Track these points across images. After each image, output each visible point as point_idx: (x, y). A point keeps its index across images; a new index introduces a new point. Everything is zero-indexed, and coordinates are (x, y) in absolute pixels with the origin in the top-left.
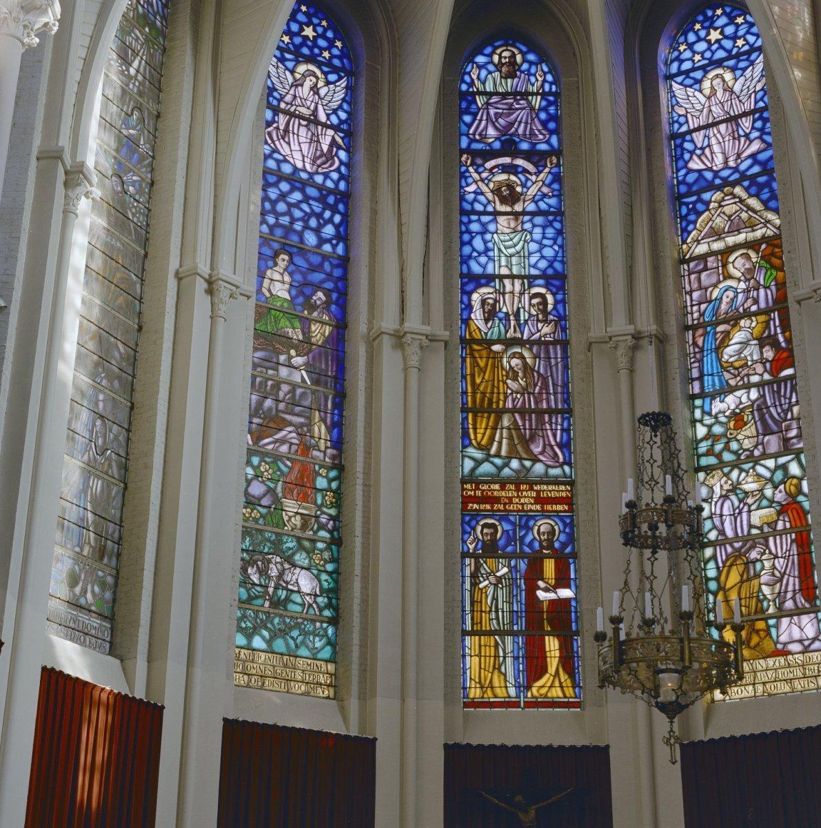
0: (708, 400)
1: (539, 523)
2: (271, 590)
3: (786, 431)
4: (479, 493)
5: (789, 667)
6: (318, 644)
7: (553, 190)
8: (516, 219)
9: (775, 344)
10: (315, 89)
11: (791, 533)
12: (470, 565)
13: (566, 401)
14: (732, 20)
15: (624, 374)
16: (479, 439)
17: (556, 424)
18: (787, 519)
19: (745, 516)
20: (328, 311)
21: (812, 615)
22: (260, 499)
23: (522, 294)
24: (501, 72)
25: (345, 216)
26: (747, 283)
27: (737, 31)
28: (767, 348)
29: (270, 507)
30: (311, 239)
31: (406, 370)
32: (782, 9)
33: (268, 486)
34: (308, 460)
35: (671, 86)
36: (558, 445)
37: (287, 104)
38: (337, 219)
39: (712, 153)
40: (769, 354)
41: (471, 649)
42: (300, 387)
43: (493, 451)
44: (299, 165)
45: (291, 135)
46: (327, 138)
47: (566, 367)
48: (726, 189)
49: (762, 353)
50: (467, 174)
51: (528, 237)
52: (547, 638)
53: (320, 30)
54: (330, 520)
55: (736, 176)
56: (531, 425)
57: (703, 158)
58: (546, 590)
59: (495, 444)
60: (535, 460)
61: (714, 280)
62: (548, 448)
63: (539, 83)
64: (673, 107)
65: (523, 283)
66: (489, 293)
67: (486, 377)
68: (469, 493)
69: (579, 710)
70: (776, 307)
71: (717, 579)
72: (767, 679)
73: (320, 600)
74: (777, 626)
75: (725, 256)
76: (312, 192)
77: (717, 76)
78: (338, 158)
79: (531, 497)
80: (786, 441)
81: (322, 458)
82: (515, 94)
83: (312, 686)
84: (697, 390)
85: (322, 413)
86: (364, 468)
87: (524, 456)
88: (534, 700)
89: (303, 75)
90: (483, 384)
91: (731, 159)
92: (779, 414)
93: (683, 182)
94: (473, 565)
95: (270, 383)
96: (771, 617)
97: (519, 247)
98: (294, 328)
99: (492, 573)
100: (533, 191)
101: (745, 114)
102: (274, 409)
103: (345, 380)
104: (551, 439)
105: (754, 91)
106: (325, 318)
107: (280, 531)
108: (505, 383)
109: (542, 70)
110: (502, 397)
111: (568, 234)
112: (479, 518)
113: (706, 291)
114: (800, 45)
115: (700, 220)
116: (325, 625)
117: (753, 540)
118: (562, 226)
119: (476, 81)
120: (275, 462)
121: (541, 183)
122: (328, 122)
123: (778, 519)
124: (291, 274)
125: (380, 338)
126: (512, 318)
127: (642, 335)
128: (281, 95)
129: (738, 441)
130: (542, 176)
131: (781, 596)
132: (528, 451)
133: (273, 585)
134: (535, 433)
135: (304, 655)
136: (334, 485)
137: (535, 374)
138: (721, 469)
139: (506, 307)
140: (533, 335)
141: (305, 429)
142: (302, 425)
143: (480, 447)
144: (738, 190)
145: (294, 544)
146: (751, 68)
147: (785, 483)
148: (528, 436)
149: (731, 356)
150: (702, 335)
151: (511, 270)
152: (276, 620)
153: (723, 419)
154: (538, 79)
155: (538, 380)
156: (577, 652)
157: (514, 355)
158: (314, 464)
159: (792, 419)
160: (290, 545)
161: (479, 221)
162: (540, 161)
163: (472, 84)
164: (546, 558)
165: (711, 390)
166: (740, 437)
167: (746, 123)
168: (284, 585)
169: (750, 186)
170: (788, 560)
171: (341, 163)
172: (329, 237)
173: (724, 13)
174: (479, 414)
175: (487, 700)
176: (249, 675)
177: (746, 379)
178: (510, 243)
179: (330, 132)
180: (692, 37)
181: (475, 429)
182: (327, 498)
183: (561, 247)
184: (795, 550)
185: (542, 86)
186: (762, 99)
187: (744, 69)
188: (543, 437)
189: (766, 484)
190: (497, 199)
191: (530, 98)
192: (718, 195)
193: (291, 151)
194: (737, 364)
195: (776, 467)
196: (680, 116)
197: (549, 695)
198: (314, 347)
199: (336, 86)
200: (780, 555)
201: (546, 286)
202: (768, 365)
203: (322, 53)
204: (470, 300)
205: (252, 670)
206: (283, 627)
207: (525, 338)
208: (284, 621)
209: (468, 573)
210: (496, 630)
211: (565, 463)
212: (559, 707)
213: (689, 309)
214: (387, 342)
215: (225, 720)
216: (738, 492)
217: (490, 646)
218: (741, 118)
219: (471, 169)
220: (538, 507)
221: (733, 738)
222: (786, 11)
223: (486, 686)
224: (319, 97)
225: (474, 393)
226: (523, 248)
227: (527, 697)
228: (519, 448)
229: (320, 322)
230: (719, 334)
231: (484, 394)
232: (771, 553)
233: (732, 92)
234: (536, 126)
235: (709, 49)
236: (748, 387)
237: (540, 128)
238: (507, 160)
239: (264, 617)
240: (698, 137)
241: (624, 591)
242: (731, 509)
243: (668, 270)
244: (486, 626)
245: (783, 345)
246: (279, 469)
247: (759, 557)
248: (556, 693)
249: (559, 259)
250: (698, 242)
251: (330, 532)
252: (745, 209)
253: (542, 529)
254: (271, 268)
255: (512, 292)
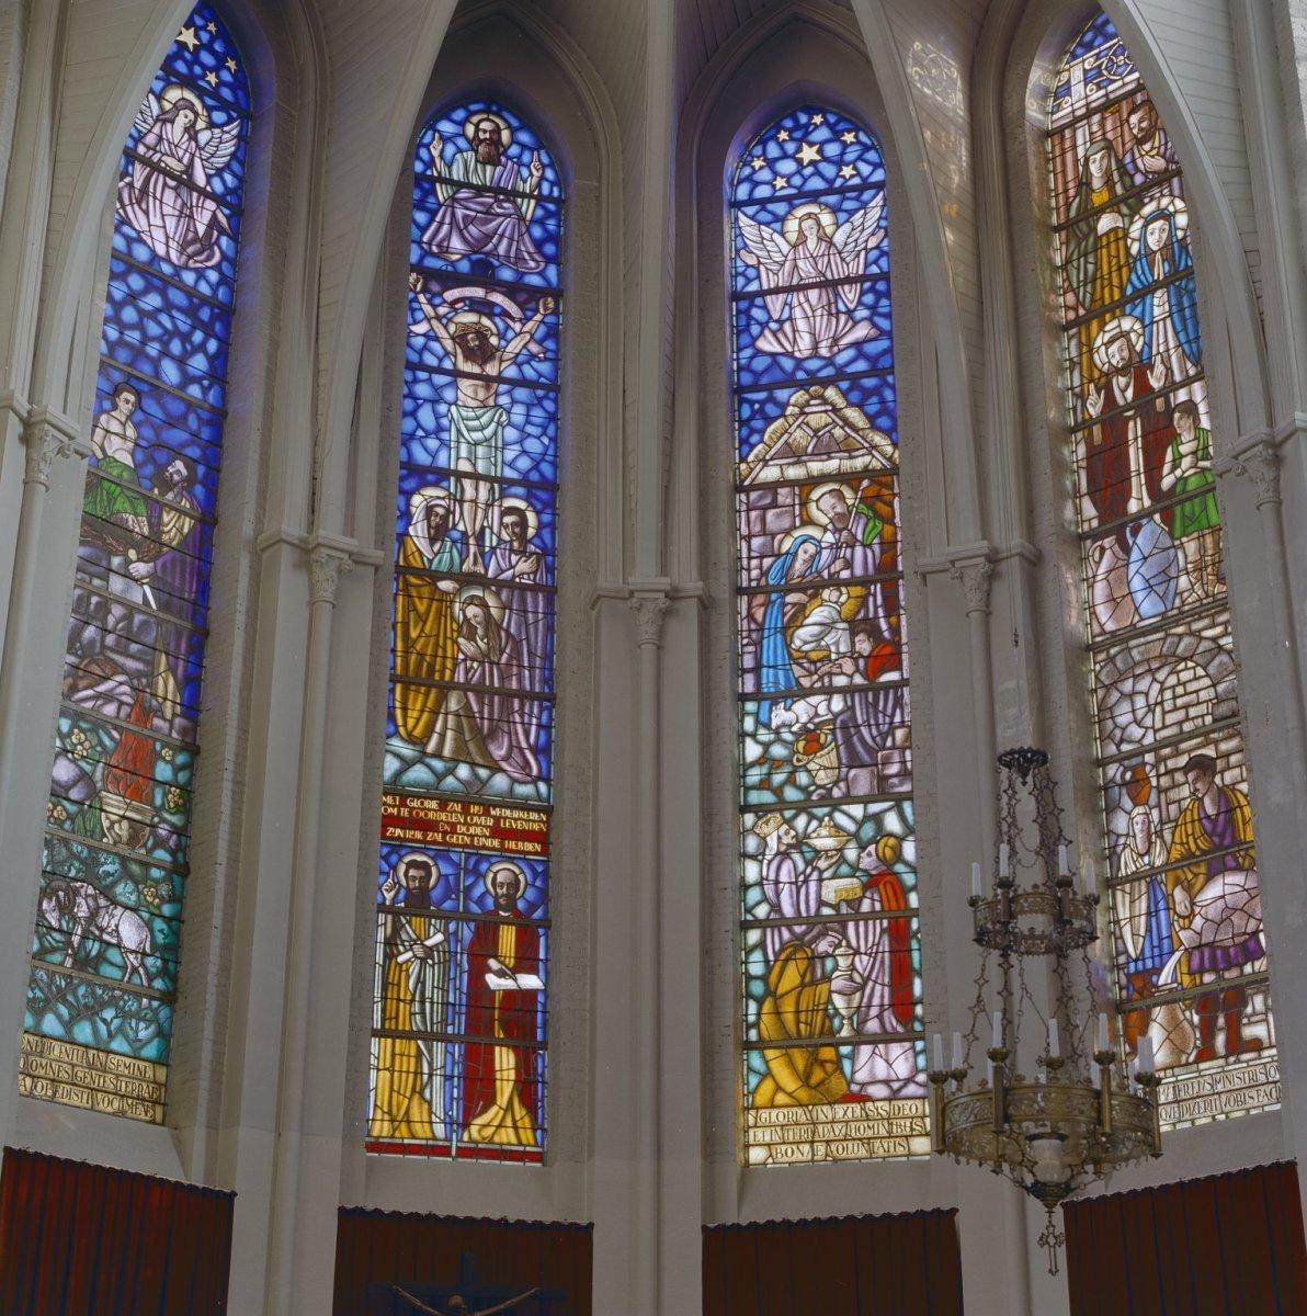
0: (766, 705)
1: (495, 868)
2: (76, 940)
3: (883, 764)
4: (405, 812)
5: (868, 1120)
6: (143, 1034)
7: (546, 350)
8: (488, 388)
9: (874, 632)
10: (191, 131)
11: (881, 919)
12: (385, 924)
13: (548, 681)
14: (836, 136)
15: (648, 652)
16: (410, 726)
17: (530, 716)
18: (876, 897)
19: (813, 886)
20: (189, 493)
21: (907, 1045)
22: (68, 788)
23: (489, 505)
24: (476, 152)
25: (224, 343)
26: (837, 536)
27: (843, 154)
28: (861, 636)
29: (83, 804)
30: (171, 373)
31: (312, 604)
32: (936, 137)
33: (81, 769)
34: (146, 732)
35: (737, 219)
36: (530, 748)
37: (148, 148)
38: (212, 346)
39: (795, 331)
40: (864, 646)
41: (378, 1058)
42: (141, 612)
43: (431, 747)
44: (161, 250)
45: (151, 199)
46: (205, 213)
47: (550, 629)
48: (813, 389)
49: (853, 643)
50: (415, 305)
51: (504, 418)
52: (497, 1049)
53: (205, 37)
54: (172, 833)
55: (829, 371)
56: (491, 712)
57: (780, 336)
58: (500, 974)
59: (435, 738)
60: (495, 769)
61: (786, 523)
62: (515, 750)
63: (535, 180)
64: (737, 251)
65: (492, 490)
66: (438, 498)
67: (427, 630)
68: (390, 810)
69: (539, 1165)
70: (878, 577)
71: (764, 978)
72: (832, 1137)
73: (150, 961)
74: (852, 1057)
75: (806, 489)
76: (177, 297)
77: (809, 215)
78: (220, 248)
79: (486, 827)
80: (882, 779)
81: (167, 732)
82: (496, 190)
83: (130, 1101)
84: (749, 687)
85: (171, 658)
86: (237, 755)
87: (479, 760)
88: (473, 1145)
89: (175, 105)
90: (422, 640)
91: (824, 344)
92: (873, 738)
93: (747, 368)
94: (389, 925)
95: (94, 600)
96: (845, 1042)
97: (488, 432)
98: (136, 515)
99: (419, 940)
100: (515, 346)
101: (848, 280)
102: (98, 645)
103: (209, 609)
104: (522, 737)
105: (865, 248)
106: (185, 503)
107: (96, 844)
108: (455, 642)
109: (540, 160)
110: (449, 664)
111: (568, 416)
112: (403, 852)
113: (773, 539)
114: (955, 193)
115: (770, 429)
116: (155, 1004)
117: (825, 923)
118: (557, 408)
119: (437, 160)
120: (94, 730)
121: (528, 336)
122: (208, 188)
123: (864, 896)
124: (137, 426)
125: (276, 547)
126: (472, 541)
127: (680, 595)
128: (139, 132)
129: (809, 771)
130: (530, 325)
131: (861, 1013)
132: (486, 754)
133: (79, 932)
134: (497, 726)
135: (121, 1050)
136: (182, 777)
137: (503, 634)
138: (781, 811)
139: (464, 523)
140: (503, 572)
141: (144, 681)
142: (139, 674)
143: (410, 739)
144: (831, 393)
145: (117, 867)
146: (862, 212)
147: (877, 843)
148: (486, 730)
149: (806, 643)
150: (761, 605)
151: (474, 465)
152: (82, 990)
153: (788, 737)
154: (532, 175)
155: (507, 643)
156: (542, 1075)
157: (471, 601)
158: (156, 740)
159: (894, 747)
160: (110, 868)
161: (429, 381)
162: (527, 301)
163: (430, 164)
164: (504, 923)
165: (772, 690)
166: (812, 766)
167: (850, 294)
168: (97, 933)
169: (850, 390)
170: (875, 958)
171: (224, 257)
172: (199, 373)
173: (826, 122)
174: (413, 687)
175: (399, 1141)
176: (33, 1077)
177: (826, 680)
178: (476, 423)
179: (210, 205)
180: (773, 150)
181: (405, 709)
182: (170, 796)
183: (553, 440)
184: (886, 945)
185: (539, 185)
186: (875, 262)
187: (851, 213)
188: (509, 734)
189: (848, 841)
190: (459, 351)
191: (519, 200)
192: (799, 396)
193: (150, 225)
194: (813, 656)
195: (864, 817)
196: (748, 266)
197: (496, 1139)
198: (165, 549)
199: (223, 132)
200: (863, 950)
201: (527, 498)
202: (861, 662)
203: (206, 75)
204: (408, 505)
205: (40, 1069)
206: (90, 1001)
207: (490, 575)
208: (94, 993)
209: (381, 937)
210: (419, 1031)
211: (540, 778)
212: (488, 1158)
213: (745, 562)
214: (286, 556)
215: (8, 1150)
216: (805, 849)
217: (409, 1056)
218: (842, 285)
219: (422, 298)
220: (496, 843)
221: (786, 1222)
222: (939, 139)
223: (399, 1118)
224: (197, 146)
225: (406, 652)
226: (495, 433)
227: (461, 1140)
228: (472, 747)
229: (177, 510)
230: (789, 607)
231: (421, 655)
232: (849, 945)
233: (831, 244)
234: (525, 245)
235: (799, 172)
236: (829, 691)
237: (532, 250)
238: (478, 292)
239: (63, 983)
240: (775, 304)
241: (976, 1010)
242: (793, 874)
243: (721, 496)
244: (404, 1025)
245: (886, 634)
246: (101, 743)
247: (830, 950)
248: (507, 1137)
249: (548, 458)
250: (766, 463)
251: (173, 853)
252: (841, 423)
253: (500, 878)
254: (108, 412)
255: (474, 501)
